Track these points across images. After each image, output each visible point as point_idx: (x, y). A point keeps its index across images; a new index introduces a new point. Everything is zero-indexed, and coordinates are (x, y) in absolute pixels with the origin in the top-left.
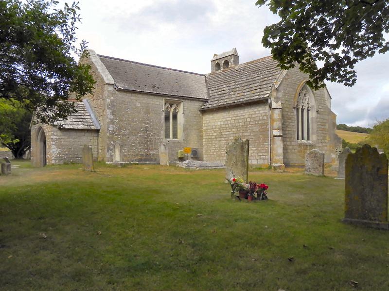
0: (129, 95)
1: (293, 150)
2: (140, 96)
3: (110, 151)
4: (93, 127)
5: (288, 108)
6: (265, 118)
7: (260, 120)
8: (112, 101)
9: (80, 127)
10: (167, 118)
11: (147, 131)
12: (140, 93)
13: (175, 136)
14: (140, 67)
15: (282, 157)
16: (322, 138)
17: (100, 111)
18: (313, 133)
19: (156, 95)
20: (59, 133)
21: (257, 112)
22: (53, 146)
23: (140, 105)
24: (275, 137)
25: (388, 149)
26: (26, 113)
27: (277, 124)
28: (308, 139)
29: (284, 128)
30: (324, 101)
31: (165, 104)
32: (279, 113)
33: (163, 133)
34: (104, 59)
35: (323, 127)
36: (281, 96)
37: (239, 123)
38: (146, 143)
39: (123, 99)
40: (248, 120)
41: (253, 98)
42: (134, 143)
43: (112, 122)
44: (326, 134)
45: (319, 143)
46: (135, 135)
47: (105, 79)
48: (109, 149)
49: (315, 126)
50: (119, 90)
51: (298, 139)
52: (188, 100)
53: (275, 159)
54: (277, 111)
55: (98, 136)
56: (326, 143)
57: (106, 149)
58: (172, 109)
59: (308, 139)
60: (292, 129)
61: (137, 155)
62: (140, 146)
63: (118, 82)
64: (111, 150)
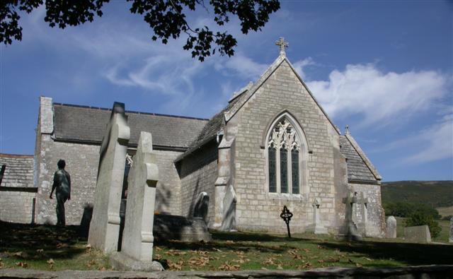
1: (247, 201)
3: (42, 213)
24: (218, 187)
25: (231, 4)
26: (101, 252)
28: (296, 191)
32: (227, 154)
36: (236, 131)
41: (397, 270)
51: (273, 189)
53: (217, 218)
56: (324, 184)
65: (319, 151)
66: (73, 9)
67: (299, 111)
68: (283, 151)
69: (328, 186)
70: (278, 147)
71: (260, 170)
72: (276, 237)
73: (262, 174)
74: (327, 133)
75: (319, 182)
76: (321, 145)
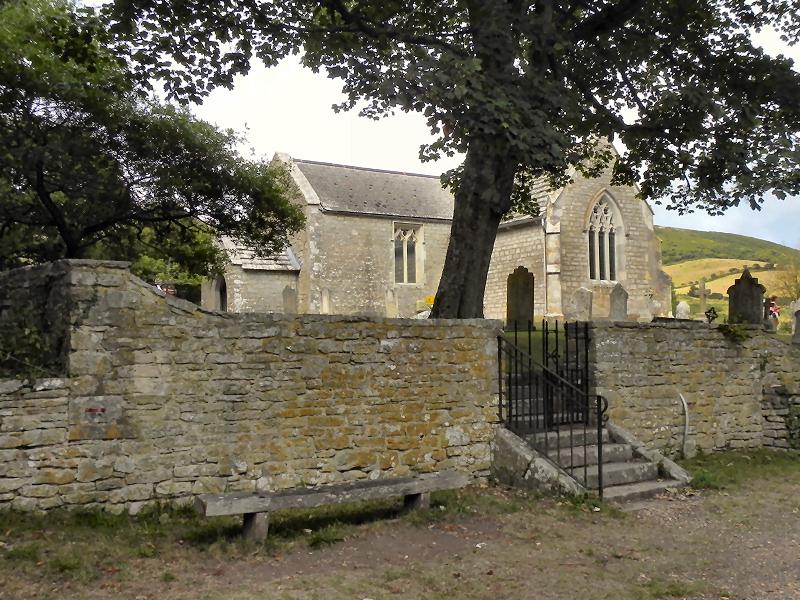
0: (341, 218)
2: (357, 219)
4: (290, 268)
5: (573, 232)
6: (539, 247)
7: (533, 250)
8: (317, 229)
9: (273, 267)
10: (398, 253)
11: (367, 271)
12: (357, 216)
13: (412, 278)
14: (358, 174)
15: (559, 304)
16: (636, 276)
17: (300, 243)
18: (620, 269)
19: (382, 218)
20: (245, 276)
21: (529, 240)
22: (237, 295)
23: (356, 234)
27: (553, 256)
28: (612, 277)
29: (562, 262)
30: (640, 218)
31: (395, 231)
33: (392, 273)
34: (305, 165)
35: (638, 259)
37: (505, 255)
38: (367, 289)
39: (333, 226)
40: (518, 251)
42: (349, 289)
43: (318, 259)
44: (643, 269)
45: (630, 284)
46: (351, 278)
47: (306, 197)
48: (313, 298)
49: (624, 257)
50: (327, 212)
52: (431, 222)
54: (553, 237)
55: (297, 280)
57: (310, 299)
58: (407, 237)
59: (612, 277)
60: (582, 264)
61: (355, 307)
62: (358, 294)
63: (325, 200)
64: (317, 299)
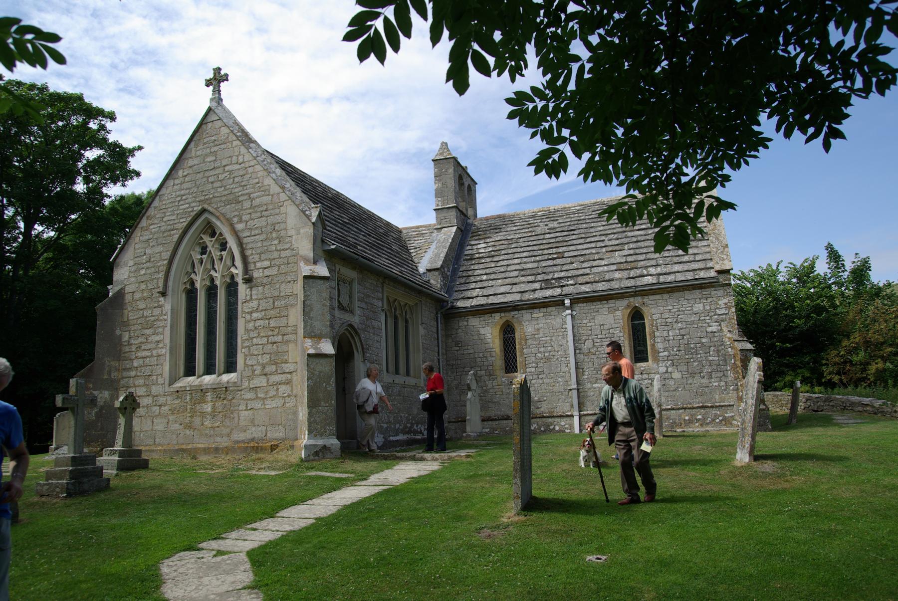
28: (231, 367)
65: (267, 272)
66: (602, 10)
67: (230, 203)
68: (211, 291)
69: (283, 348)
70: (200, 283)
71: (157, 338)
72: (692, 461)
73: (161, 345)
74: (286, 229)
75: (265, 340)
76: (271, 260)
